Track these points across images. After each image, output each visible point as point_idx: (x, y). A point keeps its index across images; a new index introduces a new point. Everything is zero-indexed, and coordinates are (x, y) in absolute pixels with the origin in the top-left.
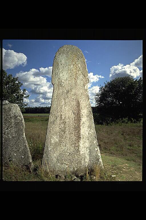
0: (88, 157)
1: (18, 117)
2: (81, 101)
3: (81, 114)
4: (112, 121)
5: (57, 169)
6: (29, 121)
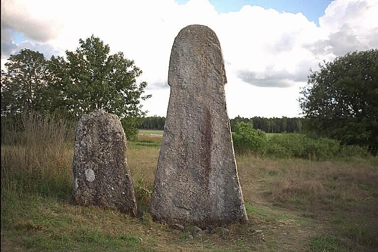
0: (222, 201)
5: (173, 215)
6: (151, 146)
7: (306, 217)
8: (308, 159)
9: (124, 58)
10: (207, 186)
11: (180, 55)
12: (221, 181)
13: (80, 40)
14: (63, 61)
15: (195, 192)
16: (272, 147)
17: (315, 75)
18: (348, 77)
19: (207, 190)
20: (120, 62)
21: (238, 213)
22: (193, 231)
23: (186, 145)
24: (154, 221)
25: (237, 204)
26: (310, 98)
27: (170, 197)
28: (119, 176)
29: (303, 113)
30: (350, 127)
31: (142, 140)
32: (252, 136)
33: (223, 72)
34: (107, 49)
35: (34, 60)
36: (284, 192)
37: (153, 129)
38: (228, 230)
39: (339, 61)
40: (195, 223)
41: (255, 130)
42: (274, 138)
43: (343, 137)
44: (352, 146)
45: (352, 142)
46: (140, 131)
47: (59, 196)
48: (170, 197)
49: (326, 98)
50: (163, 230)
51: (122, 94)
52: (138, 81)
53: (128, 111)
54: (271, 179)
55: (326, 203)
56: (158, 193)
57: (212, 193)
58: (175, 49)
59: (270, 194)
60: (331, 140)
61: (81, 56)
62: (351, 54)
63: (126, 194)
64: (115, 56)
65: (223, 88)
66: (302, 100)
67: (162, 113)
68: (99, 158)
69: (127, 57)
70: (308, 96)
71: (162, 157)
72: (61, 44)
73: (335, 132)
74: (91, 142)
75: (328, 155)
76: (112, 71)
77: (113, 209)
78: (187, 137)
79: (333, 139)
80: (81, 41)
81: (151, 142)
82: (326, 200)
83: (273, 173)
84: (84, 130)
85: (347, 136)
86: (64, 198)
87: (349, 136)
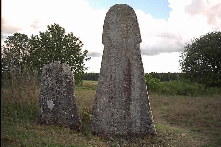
0: (139, 121)
7: (194, 131)
8: (187, 96)
9: (74, 36)
10: (129, 111)
12: (138, 107)
13: (48, 26)
14: (38, 38)
15: (121, 115)
16: (164, 89)
17: (188, 46)
18: (209, 47)
19: (129, 114)
20: (72, 38)
21: (150, 129)
22: (120, 141)
24: (93, 135)
25: (150, 123)
26: (185, 60)
27: (104, 118)
29: (182, 69)
30: (211, 76)
31: (86, 86)
32: (152, 82)
33: (139, 34)
34: (64, 31)
35: (22, 39)
36: (176, 115)
37: (92, 80)
38: (144, 141)
39: (203, 37)
40: (121, 136)
41: (154, 78)
42: (165, 84)
43: (207, 82)
44: (213, 88)
45: (212, 85)
46: (84, 81)
47: (31, 119)
48: (104, 118)
49: (195, 59)
50: (99, 141)
51: (74, 58)
52: (83, 49)
53: (76, 68)
54: (166, 107)
55: (203, 122)
56: (96, 116)
57: (132, 116)
58: (107, 20)
59: (168, 116)
60: (200, 84)
61: (49, 35)
62: (210, 33)
64: (69, 35)
65: (139, 45)
66: (181, 61)
67: (97, 70)
68: (56, 93)
69: (76, 35)
70: (185, 59)
71: (98, 93)
72: (34, 27)
73: (201, 79)
74: (50, 82)
75: (198, 93)
76: (67, 44)
77: (66, 127)
79: (200, 83)
80: (49, 27)
81: (91, 87)
82: (204, 120)
83: (166, 104)
84: (47, 74)
85: (209, 82)
86: (34, 120)
87: (210, 82)
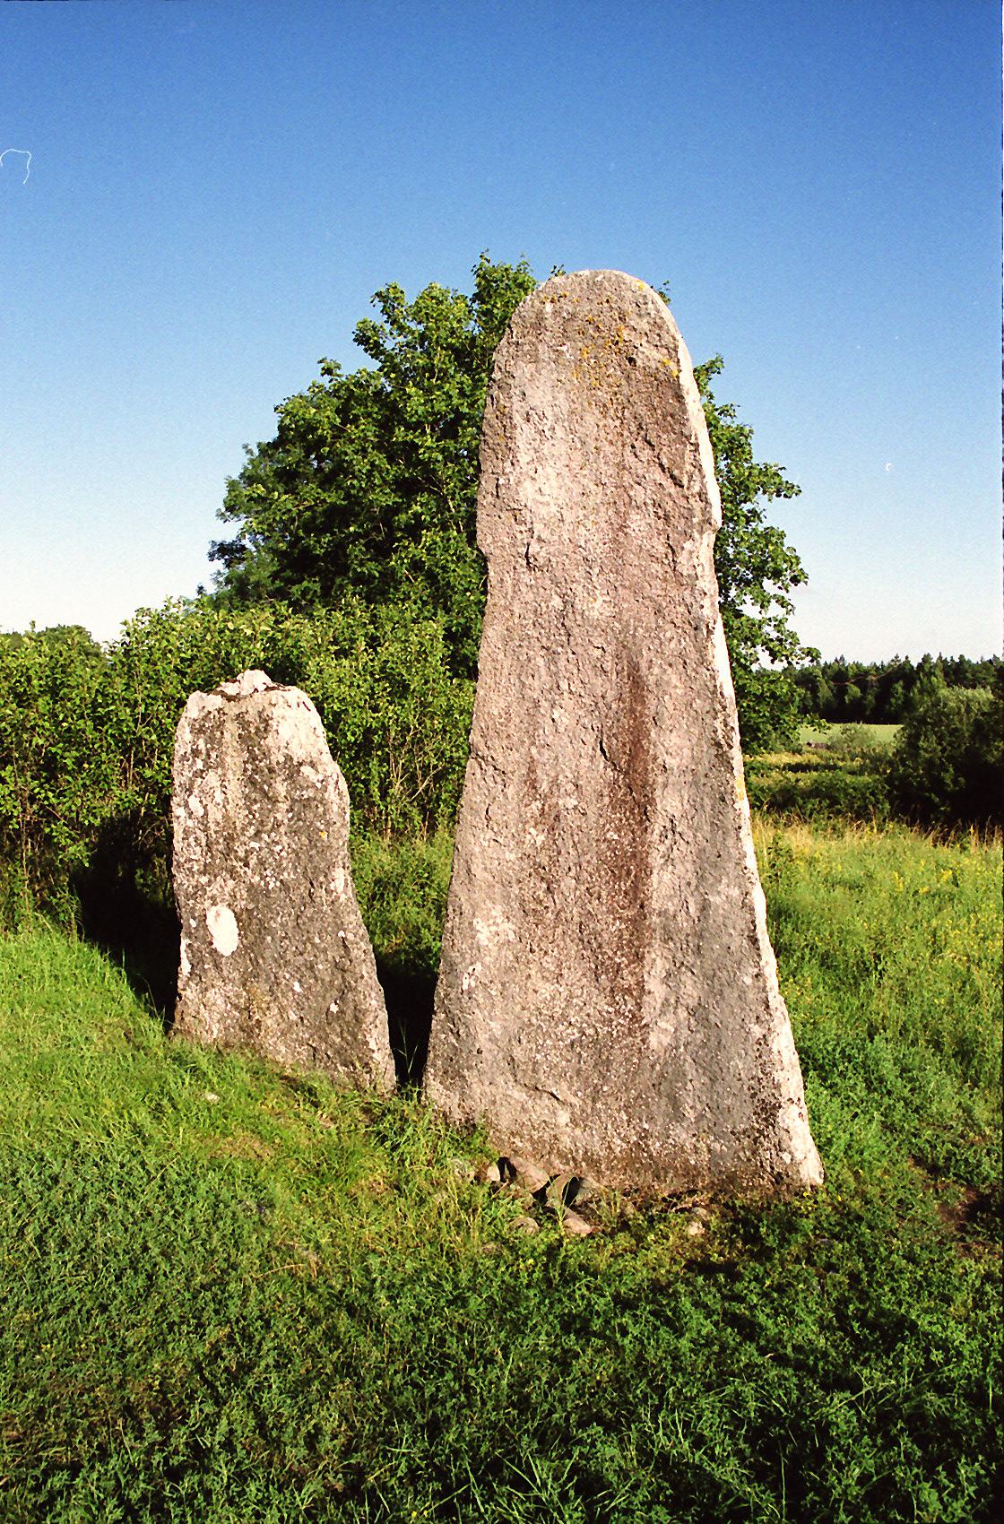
1: (306, 770)
2: (656, 670)
3: (655, 759)
4: (867, 673)
11: (518, 419)
23: (551, 820)
27: (493, 1039)
28: (317, 940)
48: (493, 1039)
52: (356, 363)
63: (342, 1012)
68: (246, 865)
78: (555, 782)
